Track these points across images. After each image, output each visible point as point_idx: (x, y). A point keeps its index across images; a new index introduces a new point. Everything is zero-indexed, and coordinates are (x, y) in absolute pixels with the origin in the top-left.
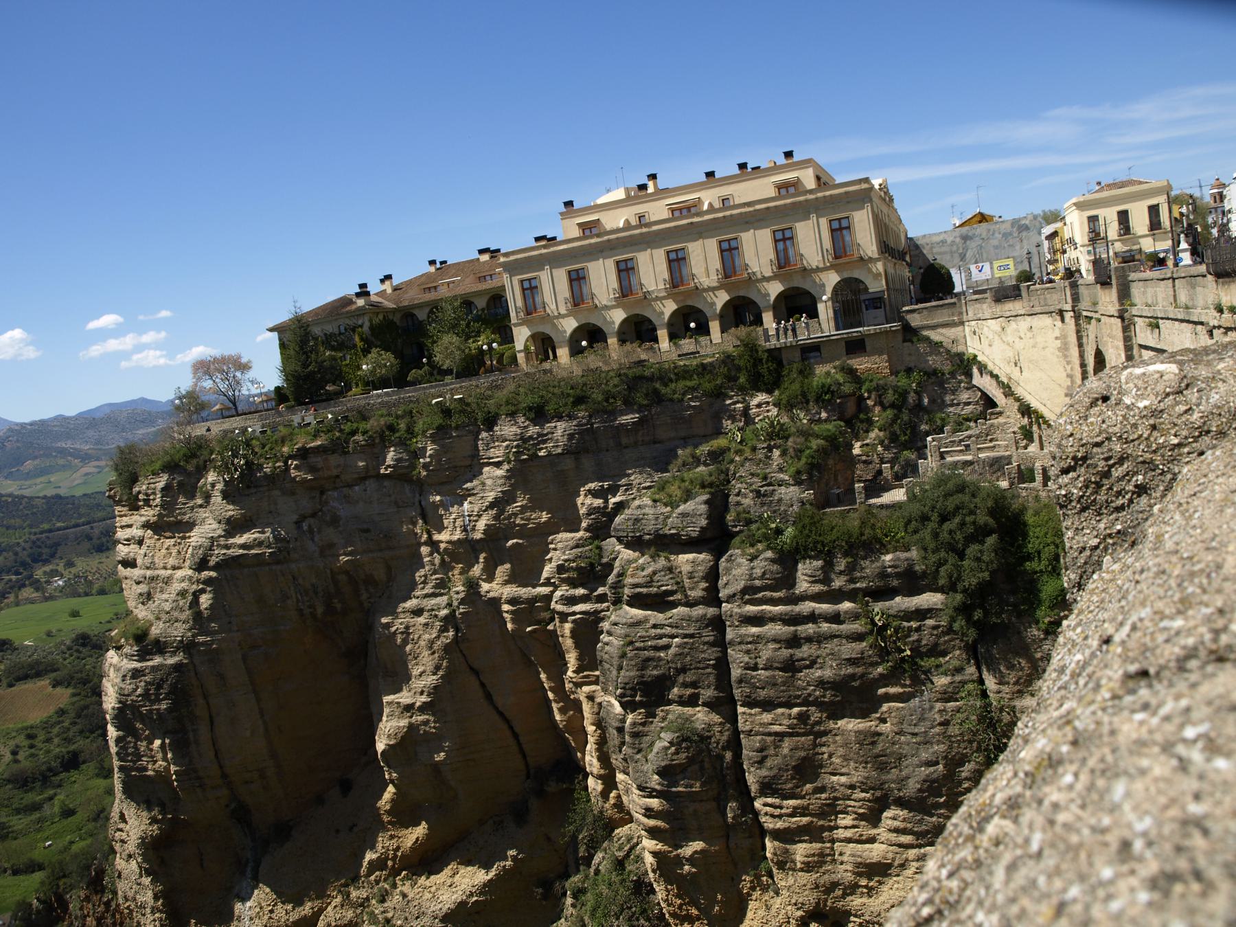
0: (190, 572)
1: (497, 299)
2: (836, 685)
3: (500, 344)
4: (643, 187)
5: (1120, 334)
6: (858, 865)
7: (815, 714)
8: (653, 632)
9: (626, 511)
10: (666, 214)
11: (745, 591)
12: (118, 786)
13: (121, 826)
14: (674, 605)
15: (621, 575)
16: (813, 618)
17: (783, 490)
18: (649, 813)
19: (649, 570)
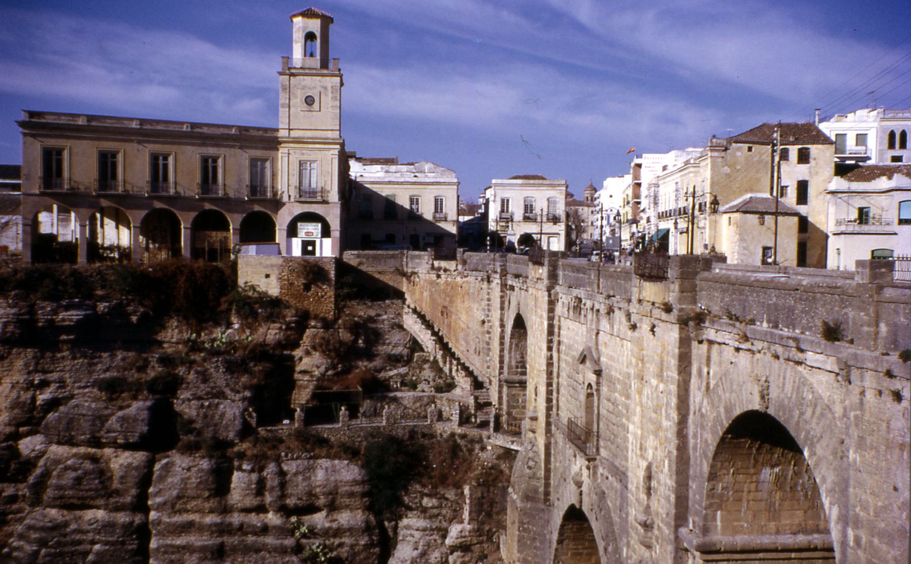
5: (546, 306)
9: (62, 408)
15: (46, 474)
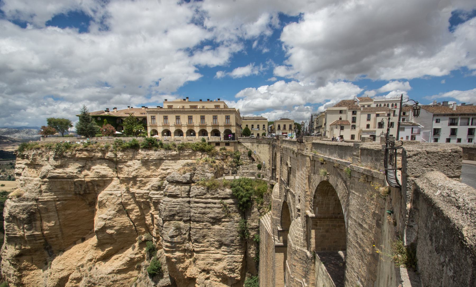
0: (40, 179)
1: (145, 119)
2: (213, 218)
3: (123, 130)
4: (184, 100)
6: (214, 259)
7: (209, 224)
8: (173, 203)
10: (189, 107)
11: (196, 196)
12: (5, 239)
13: (5, 251)
14: (179, 197)
16: (209, 203)
17: (207, 174)
18: (167, 246)
19: (174, 189)
